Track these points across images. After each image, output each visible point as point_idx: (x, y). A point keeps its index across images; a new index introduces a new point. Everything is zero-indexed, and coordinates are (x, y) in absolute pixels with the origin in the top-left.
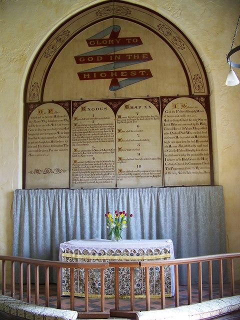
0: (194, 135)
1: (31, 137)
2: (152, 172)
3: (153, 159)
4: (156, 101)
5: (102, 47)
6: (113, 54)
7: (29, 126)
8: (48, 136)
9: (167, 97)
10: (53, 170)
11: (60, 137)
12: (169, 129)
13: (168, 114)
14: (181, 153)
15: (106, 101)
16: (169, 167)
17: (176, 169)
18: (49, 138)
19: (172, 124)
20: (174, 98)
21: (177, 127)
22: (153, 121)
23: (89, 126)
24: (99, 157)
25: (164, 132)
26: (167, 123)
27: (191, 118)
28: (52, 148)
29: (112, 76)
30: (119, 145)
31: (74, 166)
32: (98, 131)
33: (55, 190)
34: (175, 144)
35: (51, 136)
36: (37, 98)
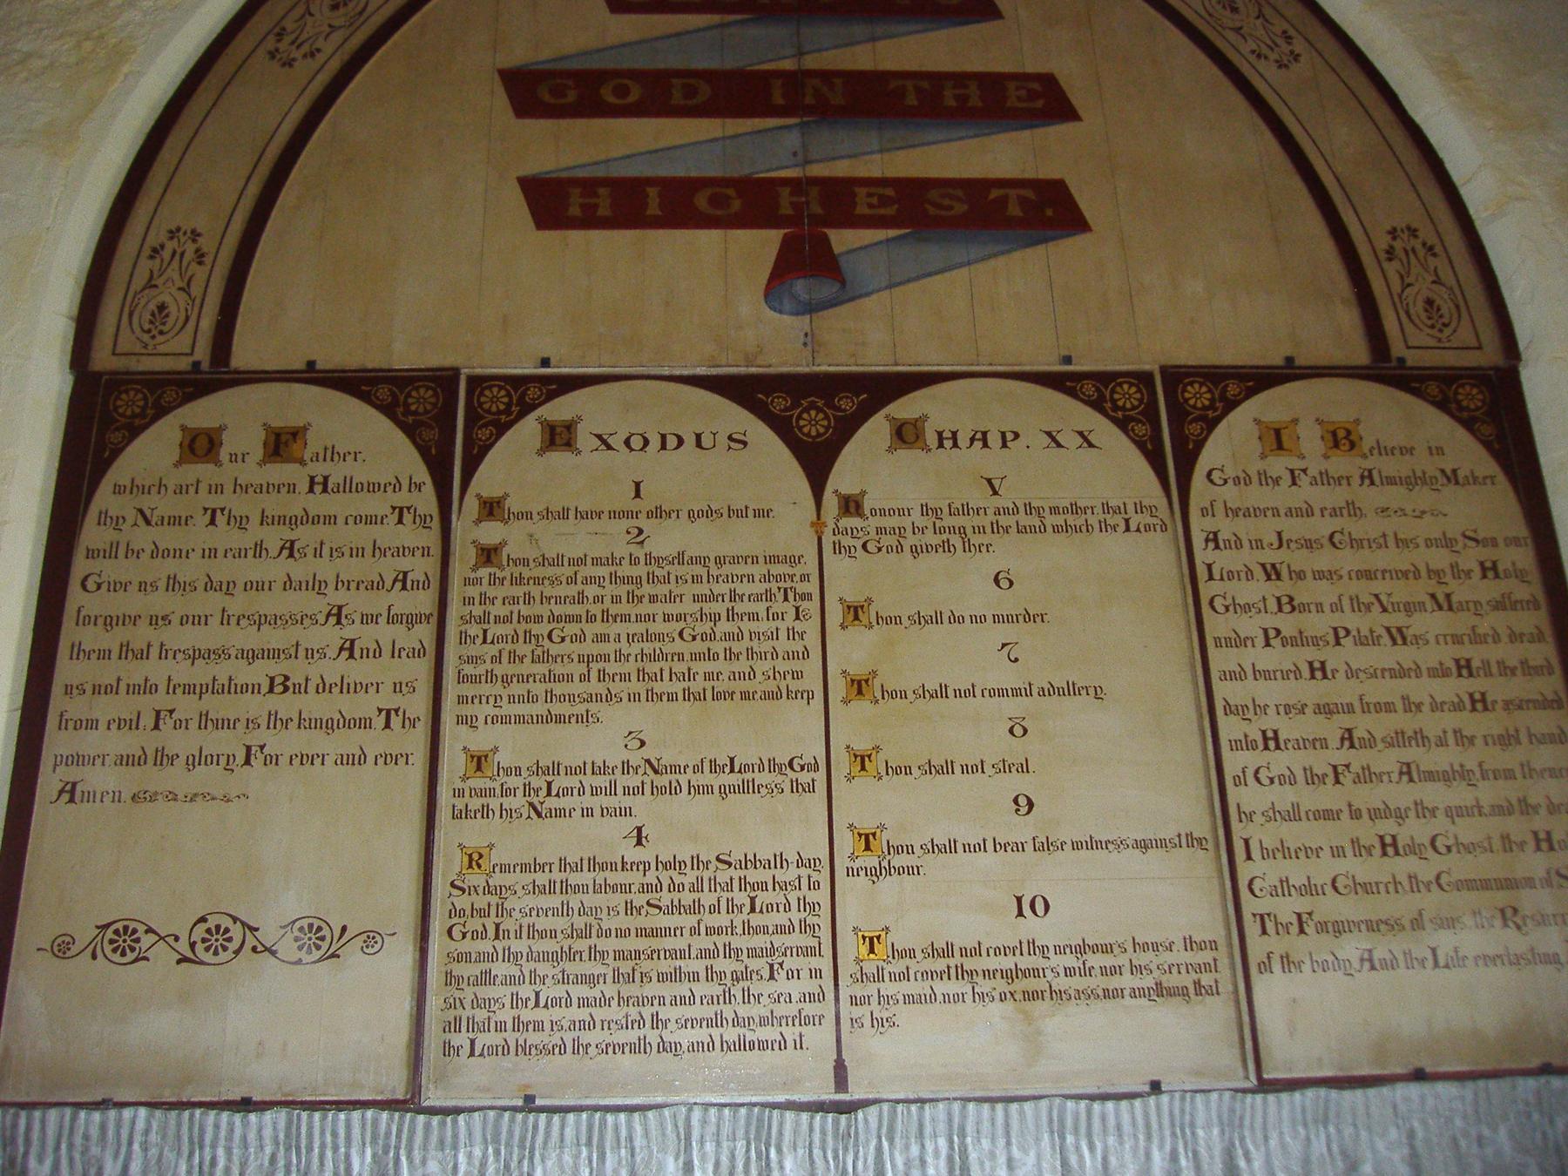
0: (1446, 654)
1: (92, 637)
2: (1142, 958)
3: (1143, 846)
4: (1128, 396)
5: (715, 19)
6: (787, 65)
7: (91, 554)
8: (247, 637)
9: (1214, 376)
10: (268, 935)
11: (349, 648)
12: (1247, 608)
13: (1230, 494)
14: (1368, 797)
15: (745, 390)
16: (1286, 908)
17: (1338, 929)
18: (251, 656)
19: (1272, 572)
20: (1260, 379)
21: (1305, 592)
22: (1115, 545)
23: (603, 571)
24: (686, 826)
25: (1216, 626)
26: (1224, 560)
27: (1407, 528)
28: (277, 742)
29: (952, 103)
30: (855, 725)
31: (462, 902)
32: (672, 609)
33: (282, 1115)
34: (1311, 725)
35: (274, 638)
36: (182, 342)
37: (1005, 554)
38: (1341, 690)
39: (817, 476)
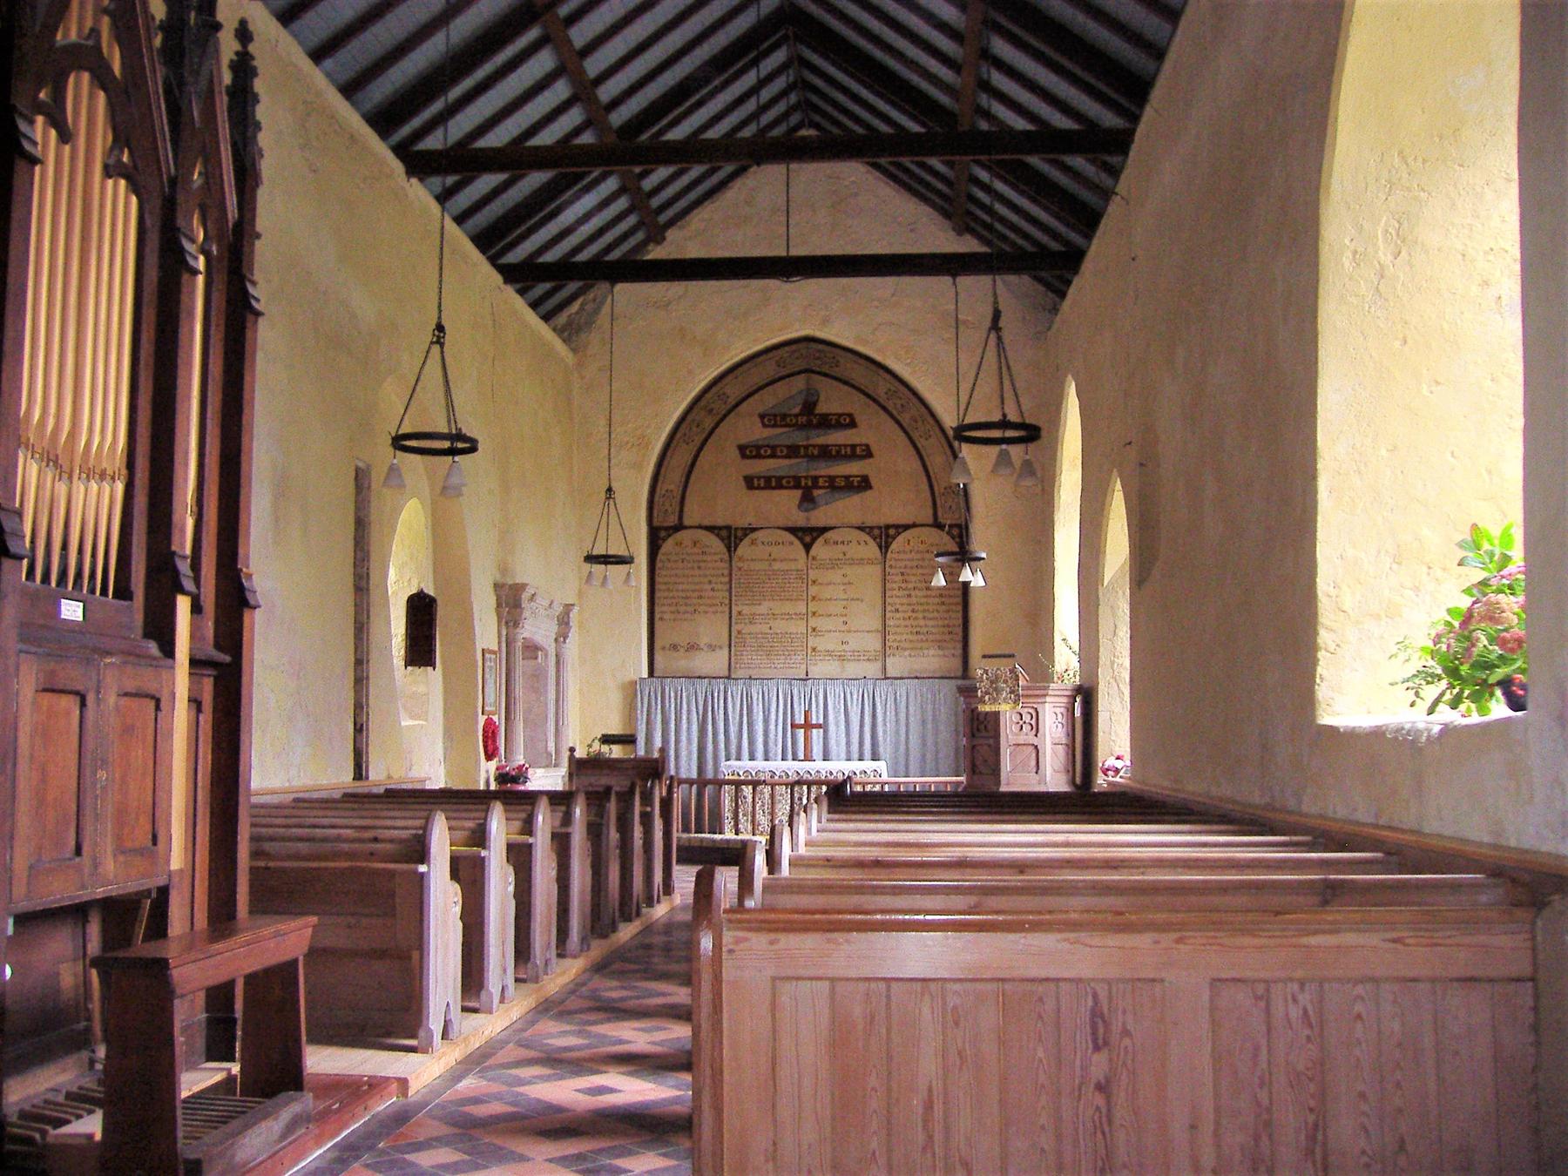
4: (876, 532)
9: (897, 527)
15: (793, 530)
20: (907, 527)
34: (905, 608)
37: (848, 570)
38: (914, 600)
39: (808, 552)
